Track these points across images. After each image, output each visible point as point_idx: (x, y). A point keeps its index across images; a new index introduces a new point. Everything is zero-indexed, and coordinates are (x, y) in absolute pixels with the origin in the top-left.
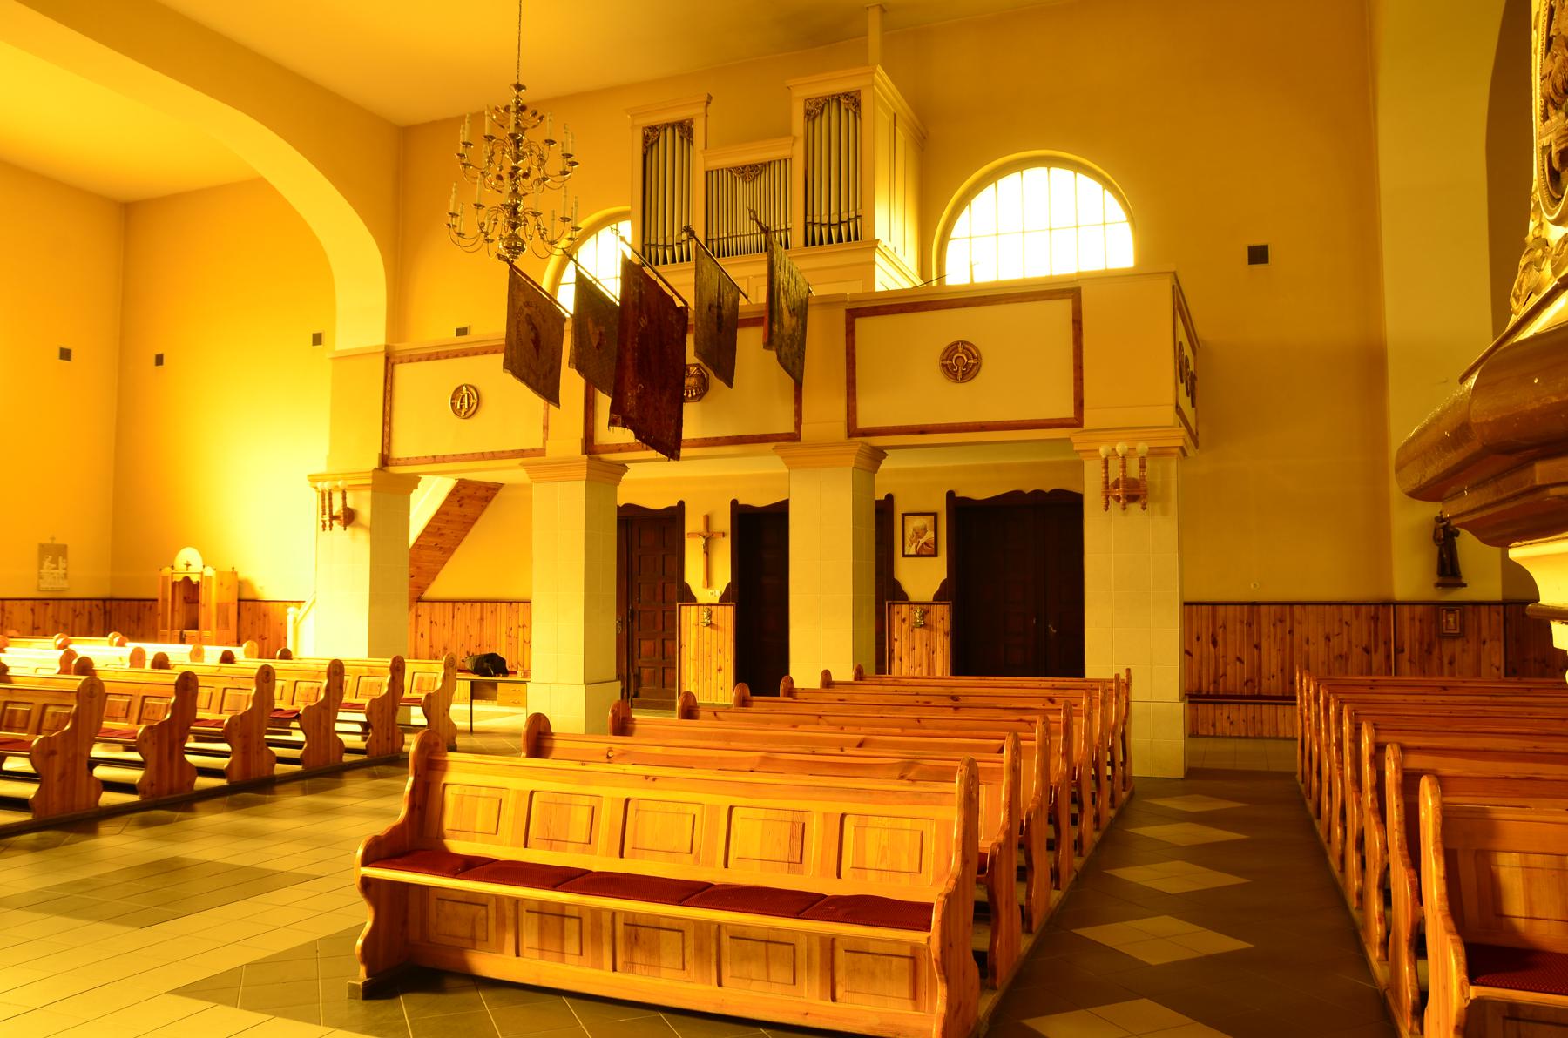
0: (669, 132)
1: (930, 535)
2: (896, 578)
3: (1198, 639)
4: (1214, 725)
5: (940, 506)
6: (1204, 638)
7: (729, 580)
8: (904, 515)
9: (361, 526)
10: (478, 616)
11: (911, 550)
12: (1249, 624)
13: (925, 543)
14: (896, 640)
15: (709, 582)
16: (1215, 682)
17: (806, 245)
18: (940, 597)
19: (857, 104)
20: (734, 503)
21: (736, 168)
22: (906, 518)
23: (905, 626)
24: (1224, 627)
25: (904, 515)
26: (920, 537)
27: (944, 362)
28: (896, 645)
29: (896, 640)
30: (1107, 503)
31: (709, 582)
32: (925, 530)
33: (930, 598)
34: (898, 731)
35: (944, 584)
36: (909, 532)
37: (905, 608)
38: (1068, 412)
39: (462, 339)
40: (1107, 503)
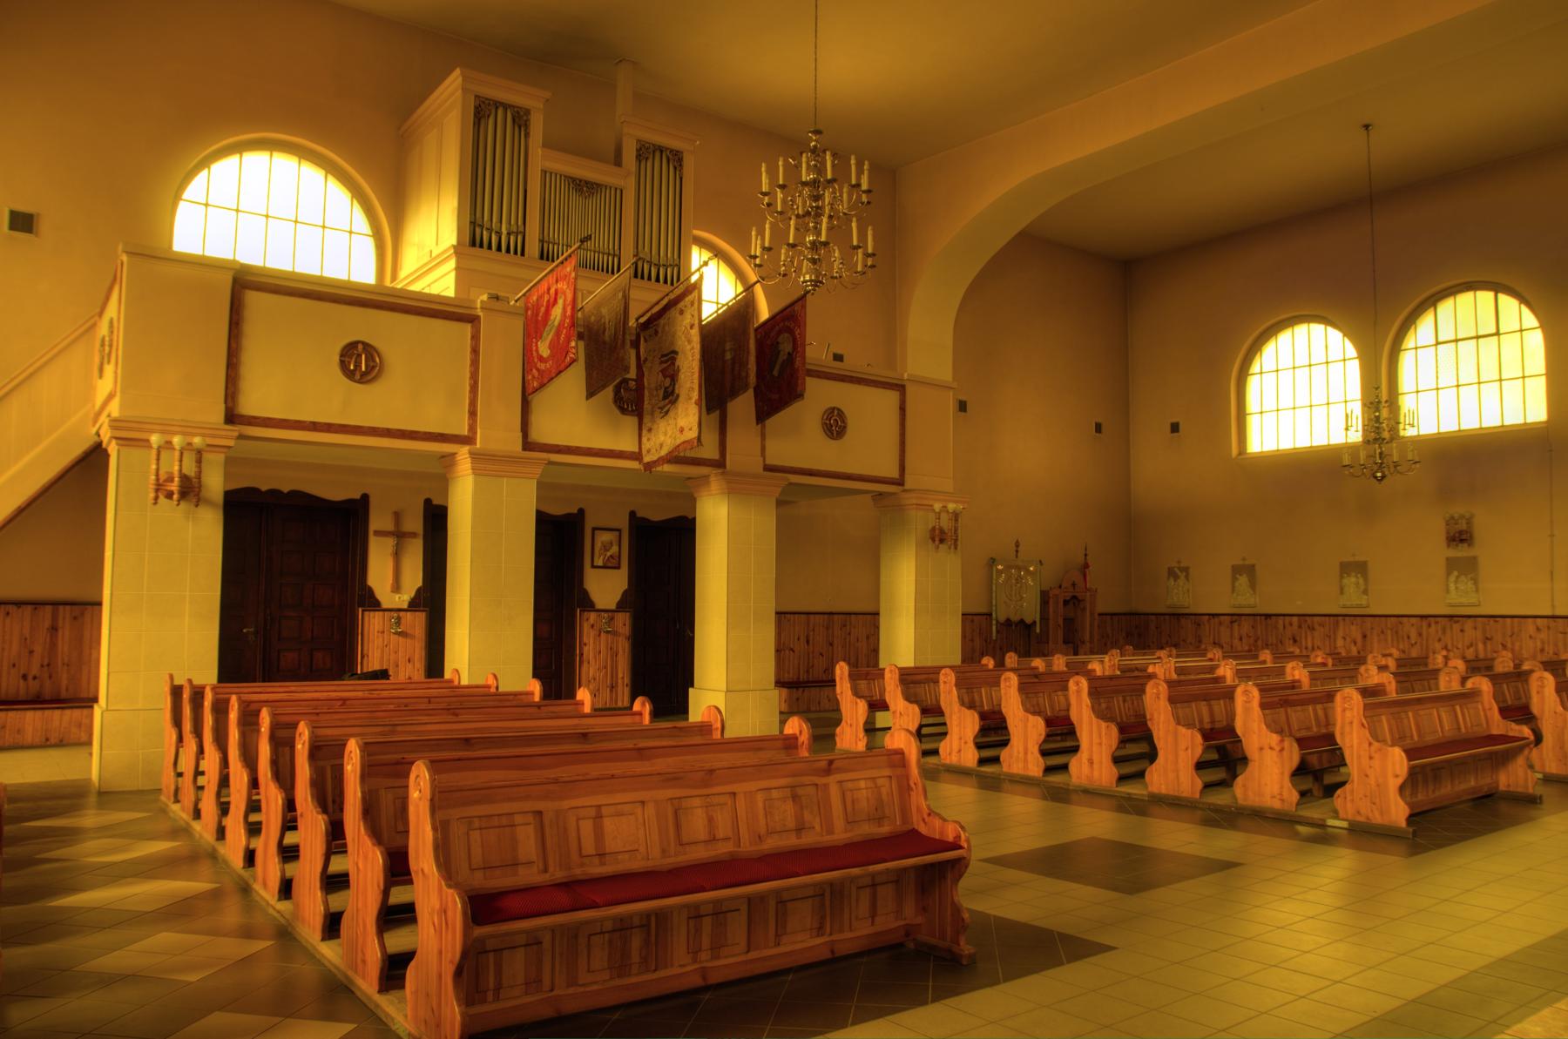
0: (500, 112)
1: (615, 549)
2: (585, 587)
3: (798, 639)
4: (819, 703)
5: (624, 524)
6: (802, 638)
7: (420, 583)
8: (594, 529)
9: (209, 503)
10: (47, 623)
11: (599, 562)
12: (827, 628)
13: (611, 556)
14: (585, 644)
15: (397, 587)
16: (808, 672)
17: (542, 258)
18: (621, 606)
19: (680, 160)
20: (632, 514)
21: (574, 180)
22: (596, 532)
23: (592, 633)
24: (814, 630)
25: (594, 529)
26: (608, 551)
27: (343, 359)
28: (586, 649)
29: (585, 644)
30: (156, 498)
31: (397, 587)
32: (611, 544)
33: (613, 607)
34: (1290, 698)
35: (625, 593)
36: (598, 546)
37: (593, 616)
38: (895, 474)
39: (837, 364)
40: (156, 498)
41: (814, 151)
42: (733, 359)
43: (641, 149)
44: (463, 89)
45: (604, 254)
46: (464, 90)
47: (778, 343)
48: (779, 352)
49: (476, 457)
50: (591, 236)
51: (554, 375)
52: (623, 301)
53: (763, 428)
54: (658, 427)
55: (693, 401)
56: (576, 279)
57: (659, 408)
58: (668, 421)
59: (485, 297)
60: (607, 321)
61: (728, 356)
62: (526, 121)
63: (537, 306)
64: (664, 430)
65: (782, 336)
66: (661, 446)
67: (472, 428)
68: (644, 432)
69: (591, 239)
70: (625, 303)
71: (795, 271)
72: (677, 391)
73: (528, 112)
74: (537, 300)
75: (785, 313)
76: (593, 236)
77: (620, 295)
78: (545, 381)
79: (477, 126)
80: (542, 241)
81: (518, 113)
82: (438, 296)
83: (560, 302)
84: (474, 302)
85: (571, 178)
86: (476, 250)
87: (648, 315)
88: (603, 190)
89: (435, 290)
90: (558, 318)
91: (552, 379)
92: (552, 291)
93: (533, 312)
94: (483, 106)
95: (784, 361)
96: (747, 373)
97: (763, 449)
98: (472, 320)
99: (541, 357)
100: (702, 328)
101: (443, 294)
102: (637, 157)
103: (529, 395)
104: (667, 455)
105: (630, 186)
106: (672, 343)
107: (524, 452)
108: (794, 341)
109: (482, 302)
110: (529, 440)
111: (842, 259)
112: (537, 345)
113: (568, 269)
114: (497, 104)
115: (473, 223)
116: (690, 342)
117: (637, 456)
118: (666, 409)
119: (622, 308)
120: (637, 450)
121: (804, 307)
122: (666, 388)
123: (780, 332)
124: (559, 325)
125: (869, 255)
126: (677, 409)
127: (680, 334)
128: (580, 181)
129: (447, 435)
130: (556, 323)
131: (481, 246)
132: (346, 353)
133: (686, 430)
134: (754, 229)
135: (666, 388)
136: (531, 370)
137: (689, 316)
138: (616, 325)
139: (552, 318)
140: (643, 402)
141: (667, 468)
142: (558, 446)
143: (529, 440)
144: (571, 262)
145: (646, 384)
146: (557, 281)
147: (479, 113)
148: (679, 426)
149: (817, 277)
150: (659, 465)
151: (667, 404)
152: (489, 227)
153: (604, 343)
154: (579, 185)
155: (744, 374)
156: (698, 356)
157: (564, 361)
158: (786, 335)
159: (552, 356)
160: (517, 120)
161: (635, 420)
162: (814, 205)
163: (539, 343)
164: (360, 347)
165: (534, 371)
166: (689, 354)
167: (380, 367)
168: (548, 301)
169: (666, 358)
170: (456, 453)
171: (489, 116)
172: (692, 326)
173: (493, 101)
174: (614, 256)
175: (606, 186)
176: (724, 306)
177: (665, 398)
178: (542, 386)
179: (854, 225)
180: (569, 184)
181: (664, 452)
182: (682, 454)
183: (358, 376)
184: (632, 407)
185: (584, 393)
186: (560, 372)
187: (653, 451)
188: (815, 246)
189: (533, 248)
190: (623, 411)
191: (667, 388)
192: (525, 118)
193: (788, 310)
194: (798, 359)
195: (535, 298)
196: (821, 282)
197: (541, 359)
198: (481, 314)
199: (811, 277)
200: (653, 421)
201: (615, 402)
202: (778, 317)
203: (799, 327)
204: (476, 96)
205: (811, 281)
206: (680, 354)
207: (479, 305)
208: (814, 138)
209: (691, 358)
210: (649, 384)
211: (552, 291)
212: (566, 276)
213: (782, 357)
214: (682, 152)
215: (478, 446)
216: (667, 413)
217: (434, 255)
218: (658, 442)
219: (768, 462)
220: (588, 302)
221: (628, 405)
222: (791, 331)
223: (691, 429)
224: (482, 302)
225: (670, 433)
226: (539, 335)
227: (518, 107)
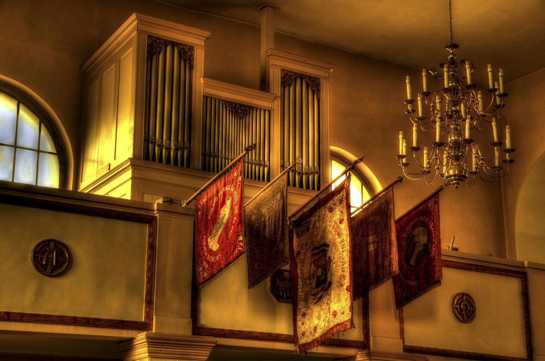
0: (169, 49)
41: (452, 62)
42: (376, 250)
43: (285, 77)
44: (137, 30)
45: (252, 164)
46: (140, 32)
47: (414, 236)
48: (415, 244)
49: (153, 342)
50: (255, 144)
51: (223, 266)
52: (281, 202)
53: (401, 312)
54: (312, 312)
55: (345, 287)
56: (242, 182)
57: (313, 295)
58: (321, 306)
59: (160, 201)
60: (267, 219)
61: (372, 248)
62: (190, 56)
63: (207, 206)
64: (317, 315)
65: (417, 230)
66: (315, 329)
67: (149, 316)
68: (299, 317)
69: (255, 147)
70: (284, 202)
71: (438, 168)
72: (329, 279)
73: (191, 48)
74: (207, 202)
75: (419, 209)
76: (257, 145)
77: (279, 196)
78: (215, 271)
79: (149, 61)
80: (204, 155)
81: (184, 49)
82: (119, 199)
83: (228, 202)
84: (152, 204)
85: (228, 102)
86: (150, 164)
87: (301, 213)
88: (255, 112)
89: (115, 195)
90: (227, 217)
91: (221, 270)
92: (221, 193)
93: (203, 212)
94: (154, 44)
95: (420, 252)
96: (390, 263)
97: (402, 332)
98: (149, 220)
99: (211, 250)
100: (351, 220)
101: (122, 198)
102: (281, 84)
103: (200, 285)
104: (321, 337)
105: (276, 106)
106: (323, 237)
107: (193, 336)
108: (429, 234)
109: (158, 204)
110: (198, 326)
111: (483, 156)
112: (207, 241)
113: (235, 174)
114: (167, 42)
115: (147, 140)
116: (339, 235)
117: (292, 339)
118: (319, 296)
119: (281, 207)
120: (292, 333)
121: (437, 203)
122: (318, 277)
123: (414, 227)
124: (228, 222)
125: (507, 151)
126: (330, 295)
127: (331, 229)
128: (236, 104)
129: (127, 322)
130: (225, 221)
131: (154, 159)
132: (40, 250)
133: (339, 313)
134: (401, 132)
135: (318, 277)
136: (202, 263)
137: (339, 213)
138: (275, 222)
139: (221, 216)
140: (298, 289)
141: (321, 350)
142: (223, 330)
143: (198, 326)
144: (237, 169)
145: (299, 274)
146: (225, 186)
147: (152, 50)
148: (332, 311)
149: (460, 172)
150: (314, 347)
151: (320, 292)
152: (160, 144)
153: (265, 237)
154: (235, 108)
155: (387, 263)
156: (347, 247)
157: (232, 254)
158: (421, 228)
159: (221, 250)
160: (183, 55)
161: (289, 306)
162: (454, 109)
163: (209, 239)
164: (52, 244)
165: (205, 263)
166: (340, 246)
167: (69, 262)
168: (217, 202)
169: (318, 250)
170: (134, 338)
171: (159, 53)
172: (341, 221)
173: (163, 39)
174: (264, 166)
175: (257, 108)
176: (358, 209)
177: (317, 286)
178: (212, 276)
179: (493, 124)
180: (226, 107)
181: (318, 335)
182: (335, 337)
183: (48, 271)
184: (286, 294)
185: (246, 283)
186: (229, 263)
187: (308, 334)
188: (457, 145)
189: (198, 162)
190: (279, 298)
191: (321, 276)
192: (189, 54)
193: (421, 207)
194: (434, 249)
195: (204, 200)
196: (464, 177)
197: (211, 252)
198: (157, 215)
199: (454, 172)
200: (307, 307)
201: (272, 291)
202: (412, 213)
203: (433, 221)
204: (149, 36)
205: (455, 175)
206: (331, 246)
207: (155, 207)
208: (451, 51)
209: (341, 250)
210: (302, 274)
211: (221, 193)
212: (233, 180)
213: (418, 249)
214: (319, 79)
215: (154, 331)
216: (320, 299)
217: (112, 168)
218: (312, 326)
219: (407, 343)
220: (250, 206)
221: (283, 293)
222: (425, 225)
223: (343, 313)
224: (158, 204)
225: (323, 317)
226: (208, 232)
227: (184, 45)
